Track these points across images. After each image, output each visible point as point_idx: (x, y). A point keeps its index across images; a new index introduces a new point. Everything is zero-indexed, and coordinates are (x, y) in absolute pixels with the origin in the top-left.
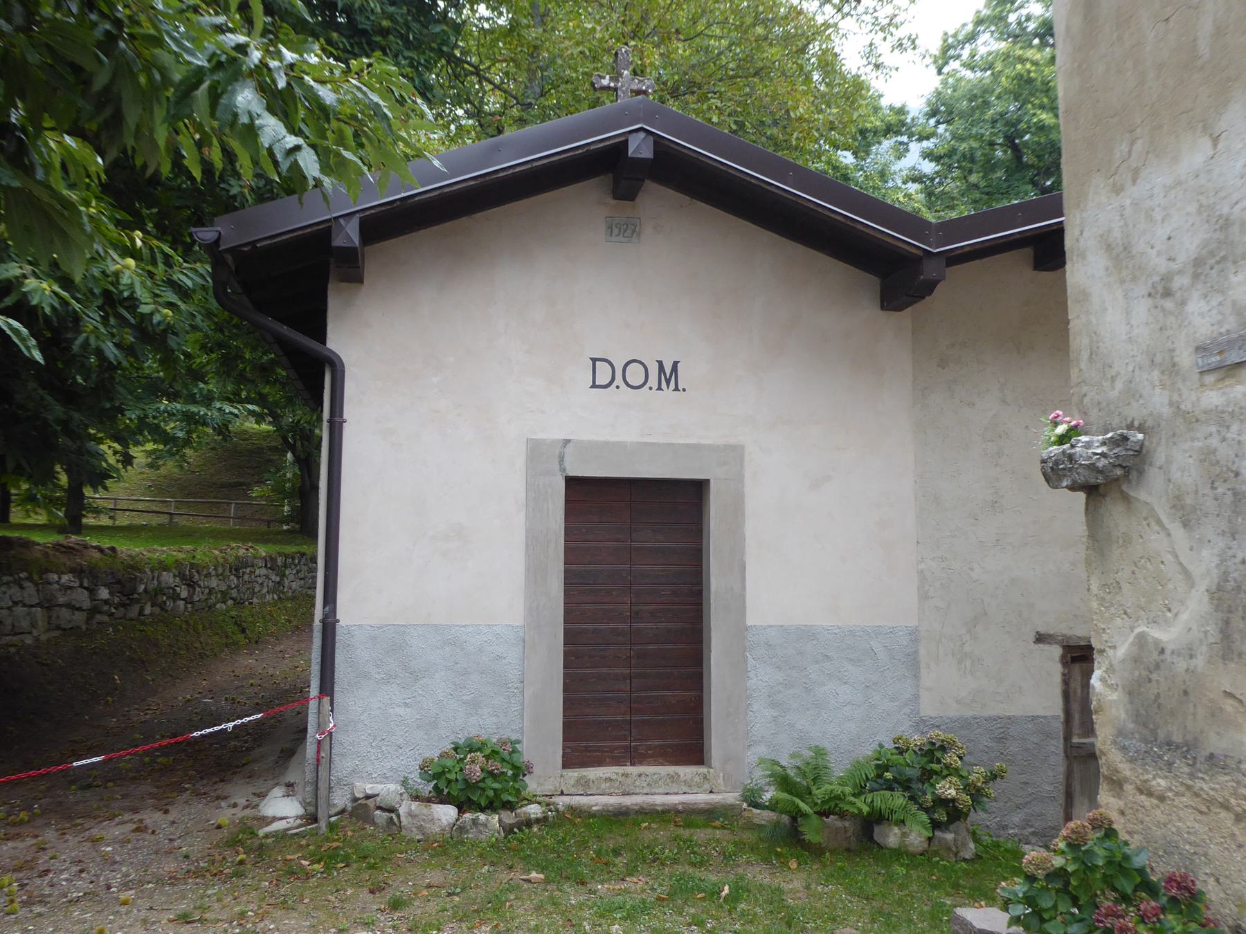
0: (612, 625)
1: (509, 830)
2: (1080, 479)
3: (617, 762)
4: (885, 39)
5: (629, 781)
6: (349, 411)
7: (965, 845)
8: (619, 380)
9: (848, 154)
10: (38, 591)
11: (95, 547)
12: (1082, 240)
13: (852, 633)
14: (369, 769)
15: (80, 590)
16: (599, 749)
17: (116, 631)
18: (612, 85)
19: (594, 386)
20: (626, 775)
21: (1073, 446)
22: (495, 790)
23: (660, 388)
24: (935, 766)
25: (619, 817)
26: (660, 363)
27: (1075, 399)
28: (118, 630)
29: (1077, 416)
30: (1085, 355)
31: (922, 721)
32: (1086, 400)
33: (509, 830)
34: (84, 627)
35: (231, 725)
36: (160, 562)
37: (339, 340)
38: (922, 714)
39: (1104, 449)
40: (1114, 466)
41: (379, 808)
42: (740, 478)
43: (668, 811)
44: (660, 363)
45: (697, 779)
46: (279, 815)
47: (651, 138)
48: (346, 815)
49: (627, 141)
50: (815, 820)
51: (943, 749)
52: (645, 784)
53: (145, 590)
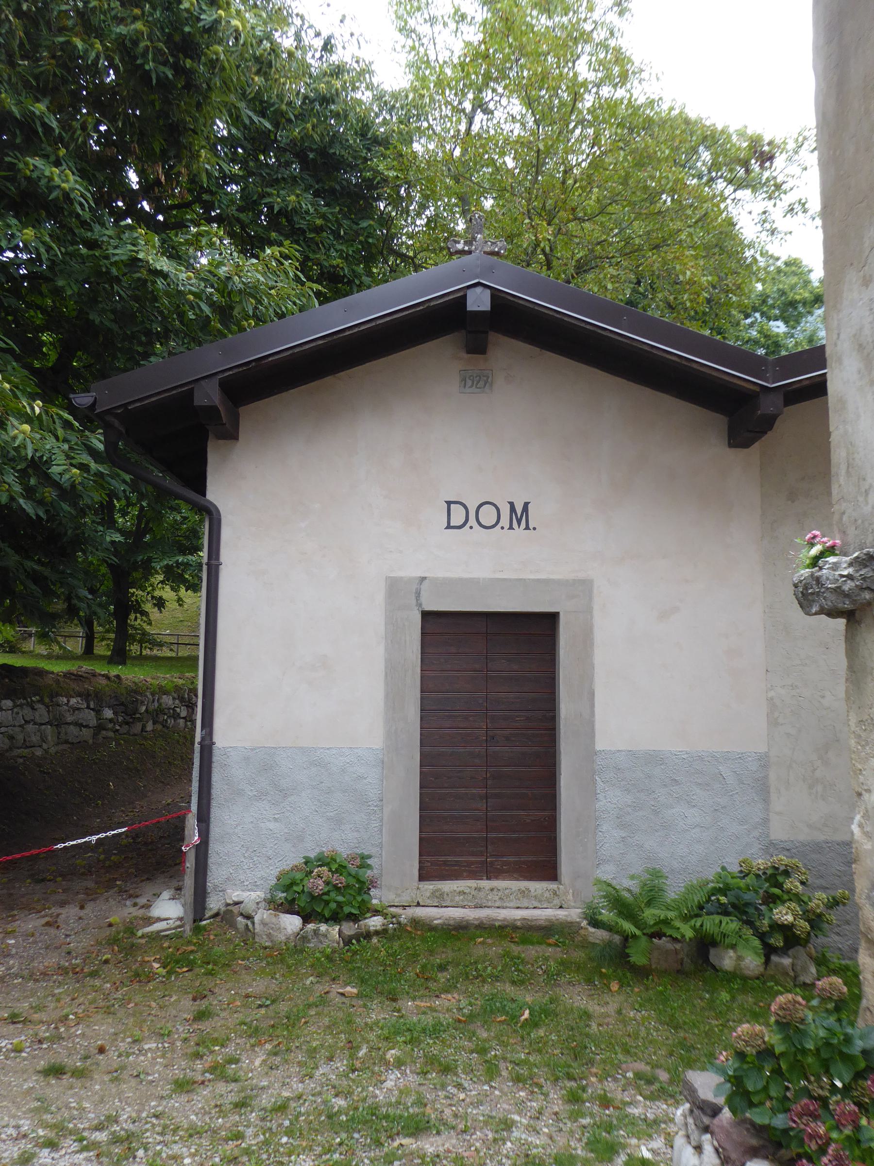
0: (469, 749)
1: (348, 941)
2: (827, 605)
3: (473, 875)
4: (775, 205)
5: (482, 894)
6: (226, 555)
7: (805, 969)
8: (472, 521)
9: (779, 323)
10: (48, 712)
11: (103, 675)
12: (839, 343)
13: (701, 758)
14: (242, 877)
15: (87, 711)
16: (457, 863)
17: (118, 744)
18: (466, 248)
19: (449, 527)
20: (478, 889)
21: (821, 568)
22: (339, 904)
23: (511, 528)
24: (776, 891)
25: (459, 931)
26: (512, 505)
27: (836, 517)
28: (120, 744)
29: (838, 536)
30: (843, 471)
31: (772, 843)
32: (845, 518)
33: (348, 941)
34: (91, 741)
35: (94, 838)
36: (161, 688)
37: (215, 493)
38: (772, 838)
39: (851, 570)
40: (862, 589)
41: (242, 914)
42: (589, 610)
43: (506, 926)
44: (512, 505)
45: (547, 894)
46: (163, 916)
47: (488, 292)
48: (218, 919)
49: (465, 296)
50: (644, 941)
51: (787, 873)
52: (497, 898)
53: (147, 711)
